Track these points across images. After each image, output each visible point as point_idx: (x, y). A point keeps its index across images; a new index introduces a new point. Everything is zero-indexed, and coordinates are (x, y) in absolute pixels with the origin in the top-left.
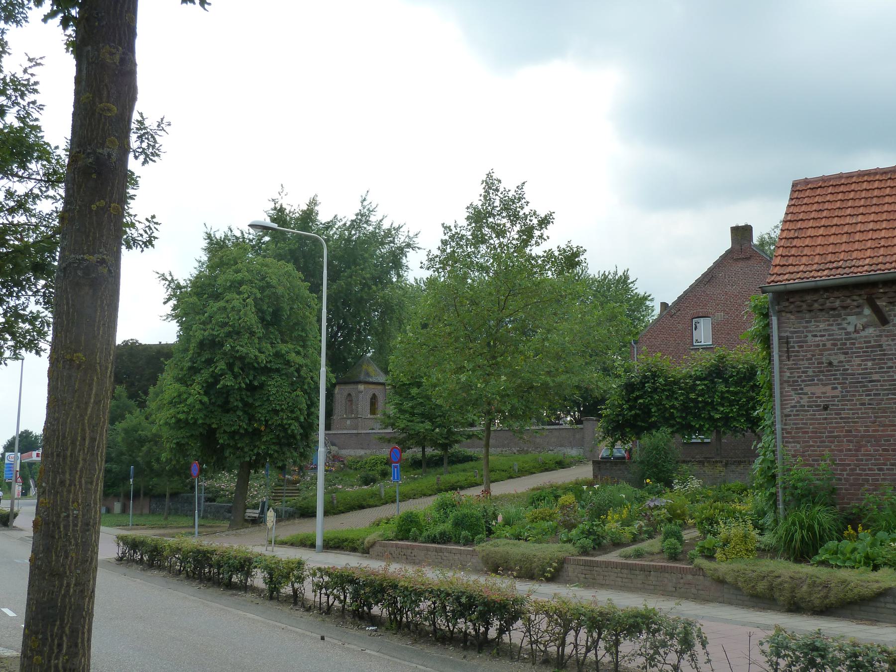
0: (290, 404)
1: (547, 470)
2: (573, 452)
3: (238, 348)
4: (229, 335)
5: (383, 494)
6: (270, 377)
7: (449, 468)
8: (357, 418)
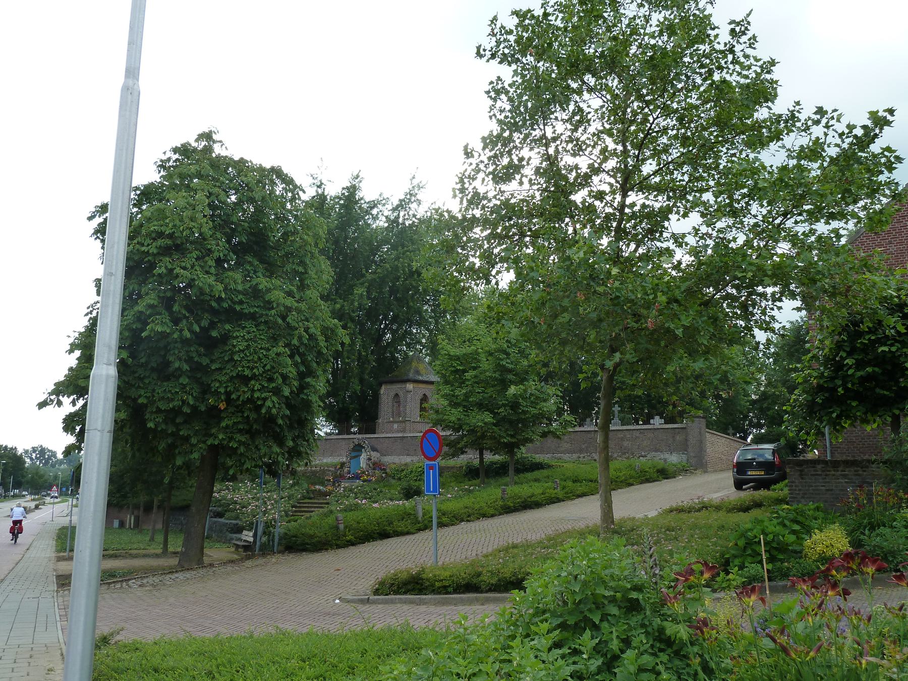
0: (268, 367)
1: (648, 481)
2: (674, 459)
3: (177, 270)
4: (166, 251)
5: (420, 514)
6: (239, 325)
7: (516, 478)
8: (404, 422)
